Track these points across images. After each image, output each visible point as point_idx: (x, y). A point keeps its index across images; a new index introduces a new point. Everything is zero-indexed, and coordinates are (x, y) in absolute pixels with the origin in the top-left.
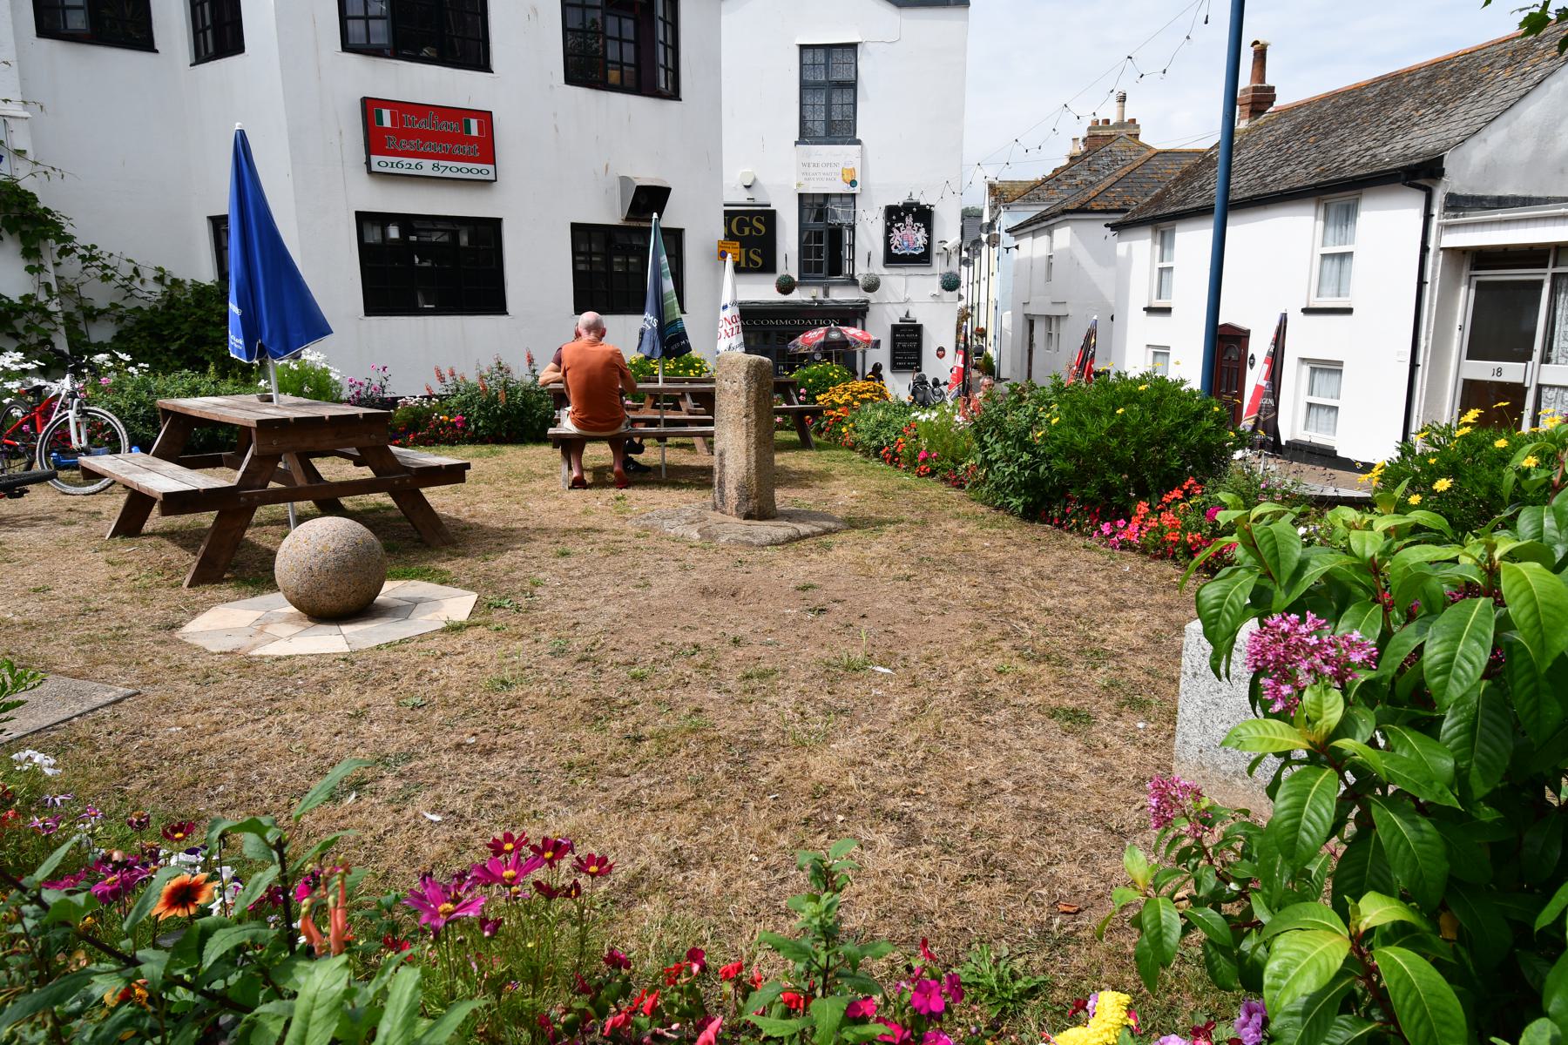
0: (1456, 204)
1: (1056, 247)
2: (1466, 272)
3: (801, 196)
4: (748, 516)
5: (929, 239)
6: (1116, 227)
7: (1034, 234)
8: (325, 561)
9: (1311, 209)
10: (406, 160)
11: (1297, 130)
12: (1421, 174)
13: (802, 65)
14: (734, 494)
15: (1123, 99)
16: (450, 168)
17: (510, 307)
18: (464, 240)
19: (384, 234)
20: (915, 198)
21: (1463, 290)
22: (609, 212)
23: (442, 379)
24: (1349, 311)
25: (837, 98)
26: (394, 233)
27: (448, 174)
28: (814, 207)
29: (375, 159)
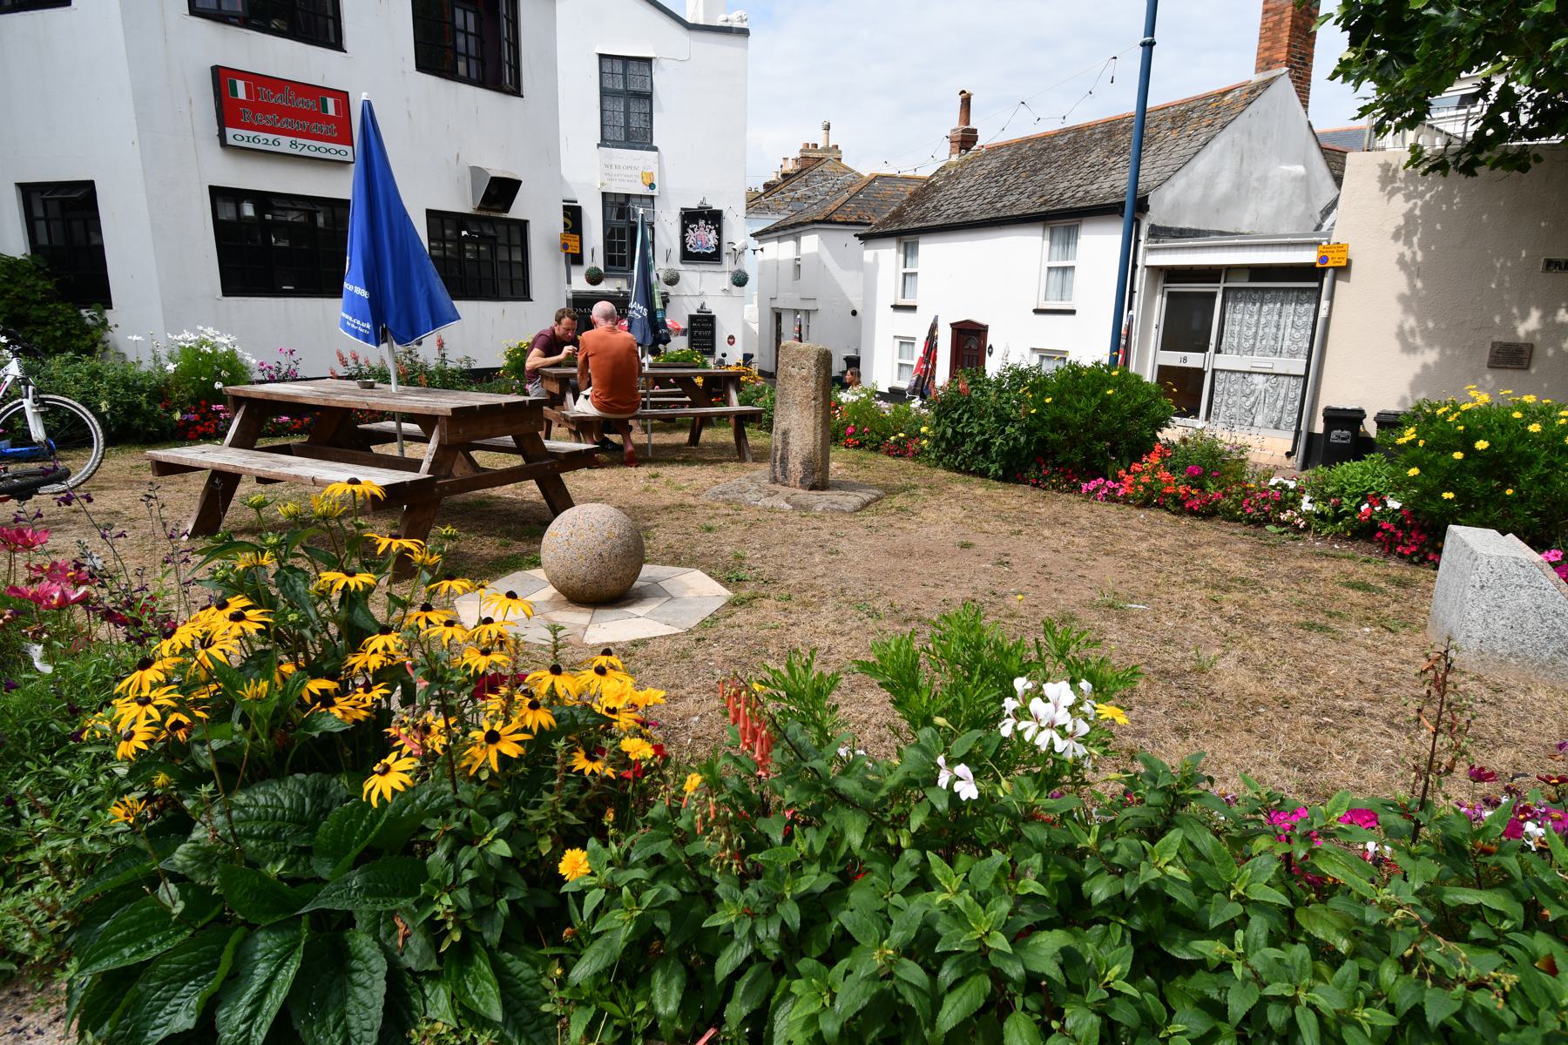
0: (1157, 232)
1: (804, 250)
2: (1160, 284)
3: (604, 195)
4: (813, 487)
5: (719, 240)
6: (864, 238)
7: (779, 239)
8: (614, 547)
9: (1040, 231)
10: (263, 135)
11: (1005, 166)
12: (1130, 210)
13: (601, 73)
14: (800, 468)
15: (828, 128)
16: (308, 147)
17: (533, 295)
18: (320, 220)
19: (238, 210)
20: (709, 203)
21: (1159, 297)
22: (462, 202)
23: (345, 364)
24: (1073, 312)
25: (635, 107)
26: (248, 210)
27: (305, 152)
28: (618, 207)
29: (230, 132)
